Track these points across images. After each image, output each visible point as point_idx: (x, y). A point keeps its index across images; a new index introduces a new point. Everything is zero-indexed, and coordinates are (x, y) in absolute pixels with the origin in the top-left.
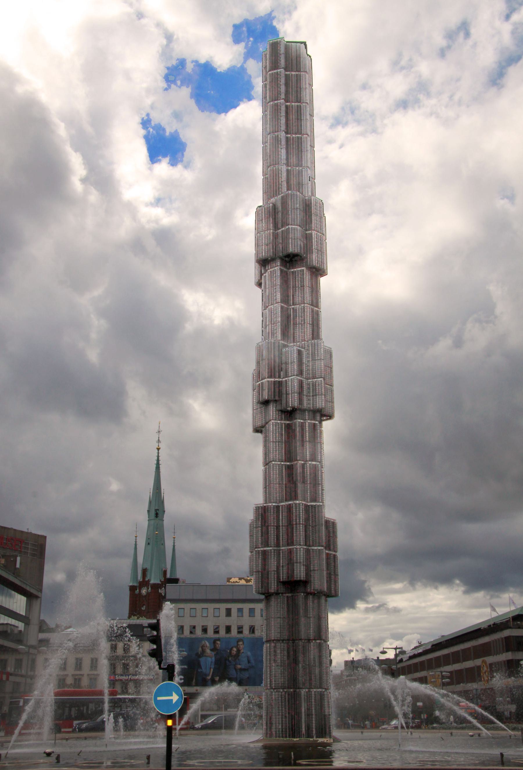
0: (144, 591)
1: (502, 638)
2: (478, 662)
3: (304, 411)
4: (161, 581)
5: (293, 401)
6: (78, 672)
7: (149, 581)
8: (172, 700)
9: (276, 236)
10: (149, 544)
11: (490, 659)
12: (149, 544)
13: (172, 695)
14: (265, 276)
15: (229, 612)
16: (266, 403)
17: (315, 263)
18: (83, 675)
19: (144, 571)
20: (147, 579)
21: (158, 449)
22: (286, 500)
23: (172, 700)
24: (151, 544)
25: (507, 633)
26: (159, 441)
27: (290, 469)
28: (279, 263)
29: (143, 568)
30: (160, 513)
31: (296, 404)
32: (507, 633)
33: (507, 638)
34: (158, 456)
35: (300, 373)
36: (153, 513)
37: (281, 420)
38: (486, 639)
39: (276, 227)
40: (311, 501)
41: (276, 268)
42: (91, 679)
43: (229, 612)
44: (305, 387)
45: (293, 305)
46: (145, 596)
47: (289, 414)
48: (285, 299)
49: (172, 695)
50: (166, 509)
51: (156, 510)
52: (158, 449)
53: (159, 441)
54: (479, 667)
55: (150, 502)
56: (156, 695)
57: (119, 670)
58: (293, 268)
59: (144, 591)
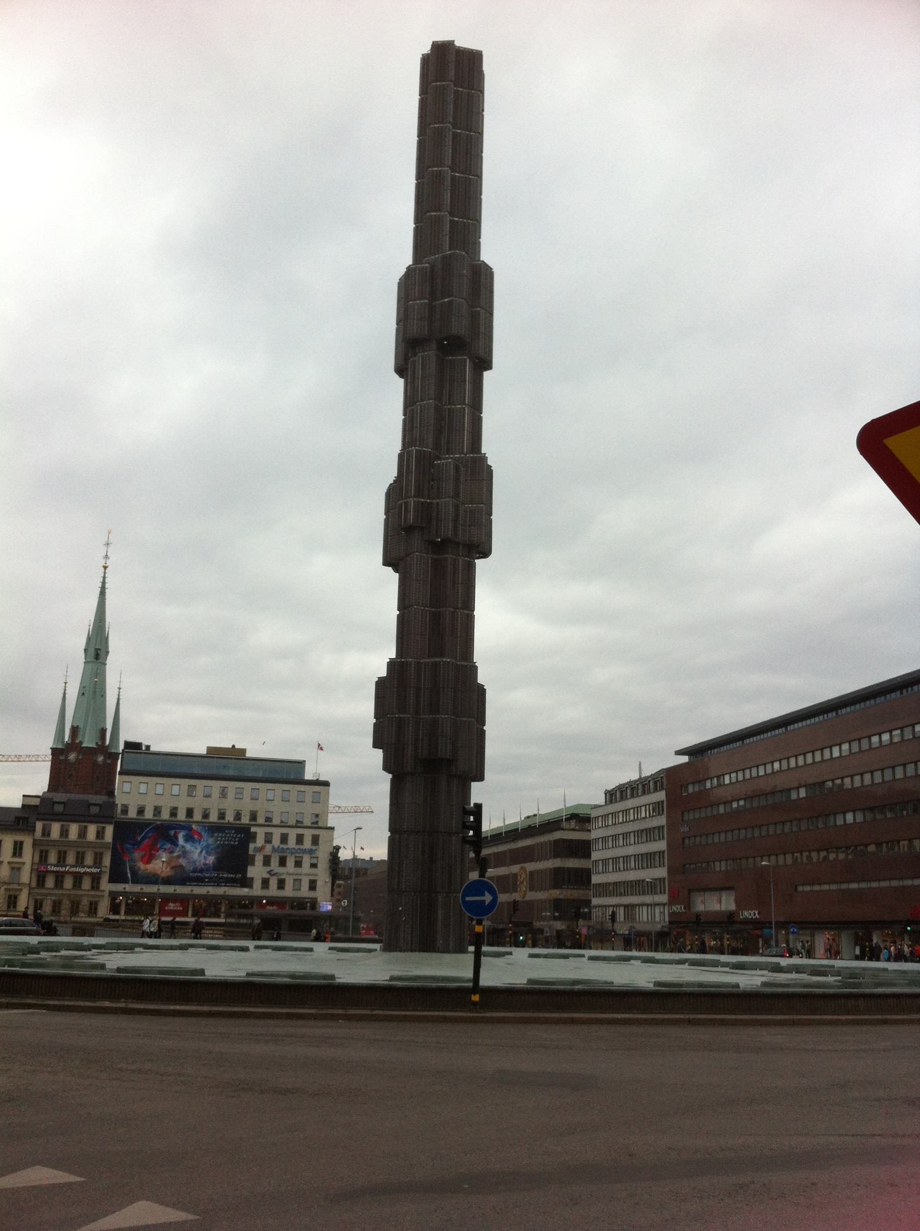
0: (72, 757)
1: (550, 842)
2: (515, 869)
3: (458, 544)
4: (97, 743)
5: (447, 530)
6: (17, 860)
7: (81, 743)
8: (484, 901)
9: (432, 309)
10: (83, 694)
11: (531, 867)
12: (83, 694)
13: (483, 895)
14: (414, 362)
15: (223, 794)
16: (409, 529)
17: (481, 353)
18: (24, 863)
19: (75, 730)
20: (77, 741)
21: (105, 568)
22: (429, 657)
23: (484, 901)
24: (86, 695)
25: (557, 835)
26: (106, 557)
27: (436, 618)
28: (434, 346)
29: (72, 726)
30: (102, 653)
31: (450, 534)
32: (557, 835)
33: (557, 842)
34: (104, 578)
35: (457, 495)
36: (92, 652)
37: (427, 553)
38: (528, 842)
39: (433, 296)
40: (460, 660)
41: (431, 353)
42: (13, 869)
43: (223, 794)
44: (461, 512)
45: (450, 404)
46: (74, 764)
47: (439, 547)
48: (439, 398)
49: (483, 895)
50: (110, 649)
51: (97, 650)
52: (105, 568)
53: (106, 557)
54: (515, 876)
55: (89, 639)
56: (464, 897)
57: (52, 858)
58: (452, 355)
59: (72, 757)
